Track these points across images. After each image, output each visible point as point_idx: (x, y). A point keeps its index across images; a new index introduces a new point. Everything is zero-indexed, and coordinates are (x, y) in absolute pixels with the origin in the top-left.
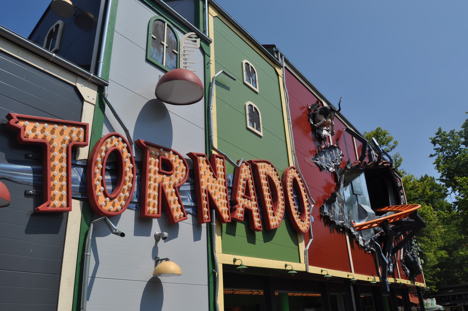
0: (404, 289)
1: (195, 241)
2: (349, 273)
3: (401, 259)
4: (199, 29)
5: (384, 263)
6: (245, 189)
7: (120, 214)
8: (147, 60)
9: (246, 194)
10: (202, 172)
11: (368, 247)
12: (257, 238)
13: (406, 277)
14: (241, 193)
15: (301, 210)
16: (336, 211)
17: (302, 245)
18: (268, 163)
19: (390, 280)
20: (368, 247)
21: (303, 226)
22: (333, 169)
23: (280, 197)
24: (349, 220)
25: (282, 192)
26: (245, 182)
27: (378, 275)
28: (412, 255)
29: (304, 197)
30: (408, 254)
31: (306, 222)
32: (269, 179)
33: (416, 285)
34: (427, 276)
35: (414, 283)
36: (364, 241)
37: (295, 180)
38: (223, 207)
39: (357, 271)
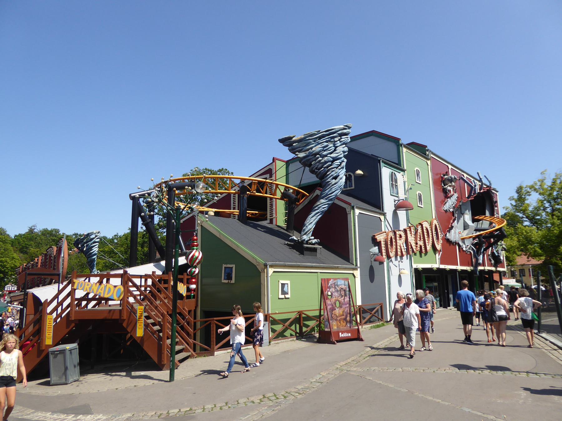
0: (490, 272)
1: (379, 265)
4: (401, 167)
8: (391, 195)
13: (491, 265)
14: (418, 239)
15: (438, 238)
17: (437, 255)
18: (427, 221)
19: (480, 268)
21: (439, 247)
23: (430, 236)
27: (472, 266)
28: (497, 251)
29: (439, 232)
30: (494, 251)
33: (498, 270)
34: (143, 214)
35: (497, 269)
36: (466, 248)
37: (436, 225)
39: (461, 265)
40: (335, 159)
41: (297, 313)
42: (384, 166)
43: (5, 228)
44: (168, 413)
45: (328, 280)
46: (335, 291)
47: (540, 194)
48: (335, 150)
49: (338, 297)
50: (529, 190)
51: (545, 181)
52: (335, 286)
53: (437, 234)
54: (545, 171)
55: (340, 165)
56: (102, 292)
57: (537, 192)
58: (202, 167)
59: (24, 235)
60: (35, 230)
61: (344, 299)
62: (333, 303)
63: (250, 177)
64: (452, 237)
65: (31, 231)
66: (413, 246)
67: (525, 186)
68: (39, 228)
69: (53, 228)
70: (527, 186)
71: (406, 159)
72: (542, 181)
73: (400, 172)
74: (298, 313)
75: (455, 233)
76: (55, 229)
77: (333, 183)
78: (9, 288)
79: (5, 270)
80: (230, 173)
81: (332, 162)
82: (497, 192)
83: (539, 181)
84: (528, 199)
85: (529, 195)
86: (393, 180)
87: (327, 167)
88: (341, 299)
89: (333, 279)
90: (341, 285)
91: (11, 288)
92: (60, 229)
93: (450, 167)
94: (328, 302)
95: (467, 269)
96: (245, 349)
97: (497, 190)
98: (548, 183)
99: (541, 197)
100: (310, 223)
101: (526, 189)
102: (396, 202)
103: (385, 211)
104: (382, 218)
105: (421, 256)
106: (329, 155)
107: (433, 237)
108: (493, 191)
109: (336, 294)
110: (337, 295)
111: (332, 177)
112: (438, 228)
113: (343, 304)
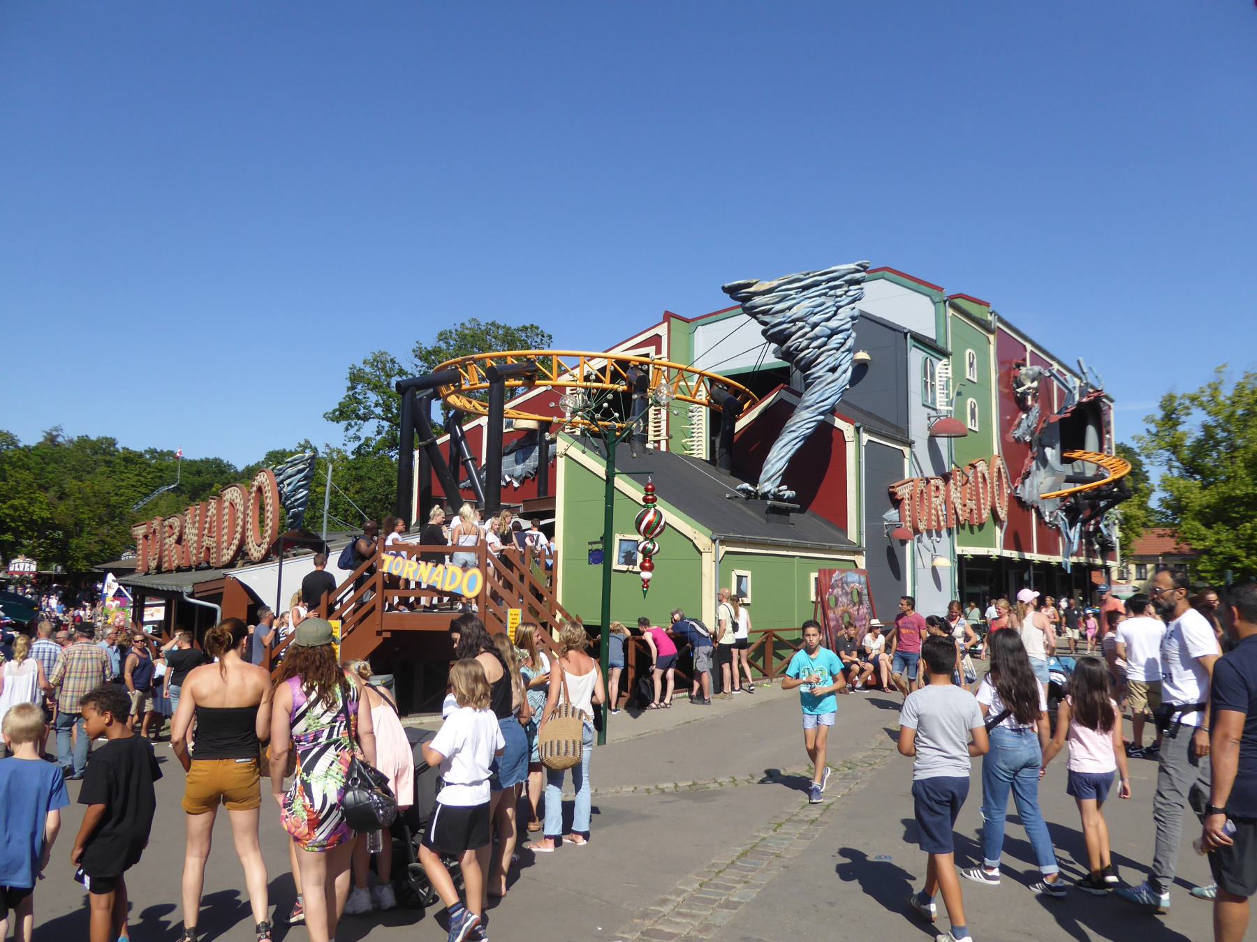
21: (1003, 514)
36: (1050, 516)
40: (835, 332)
41: (762, 633)
42: (914, 346)
43: (14, 434)
44: (676, 786)
45: (831, 572)
46: (843, 593)
47: (1209, 413)
48: (835, 314)
49: (848, 605)
50: (1187, 403)
51: (1221, 387)
52: (842, 583)
53: (1000, 486)
54: (1224, 366)
55: (843, 344)
56: (439, 580)
57: (1204, 409)
58: (484, 321)
59: (36, 448)
60: (60, 439)
61: (858, 610)
62: (838, 617)
63: (606, 351)
64: (1027, 493)
65: (51, 439)
66: (958, 510)
67: (1179, 395)
68: (71, 432)
69: (103, 435)
70: (1184, 396)
71: (952, 332)
72: (1216, 389)
73: (941, 357)
74: (766, 633)
75: (1032, 486)
76: (106, 439)
77: (829, 381)
78: (19, 567)
79: (18, 526)
80: (545, 335)
81: (830, 337)
82: (1112, 401)
83: (1209, 386)
84: (1184, 422)
85: (1188, 414)
86: (928, 373)
87: (819, 347)
88: (853, 610)
89: (839, 570)
90: (853, 582)
91: (22, 566)
92: (118, 439)
93: (1029, 347)
94: (831, 615)
95: (1012, 556)
96: (682, 697)
97: (1112, 396)
98: (1227, 392)
99: (1210, 420)
100: (779, 457)
101: (1182, 401)
102: (932, 419)
103: (913, 437)
104: (906, 450)
105: (972, 532)
106: (823, 324)
107: (993, 493)
108: (1104, 400)
109: (844, 600)
110: (845, 601)
111: (827, 368)
112: (1003, 475)
113: (855, 620)
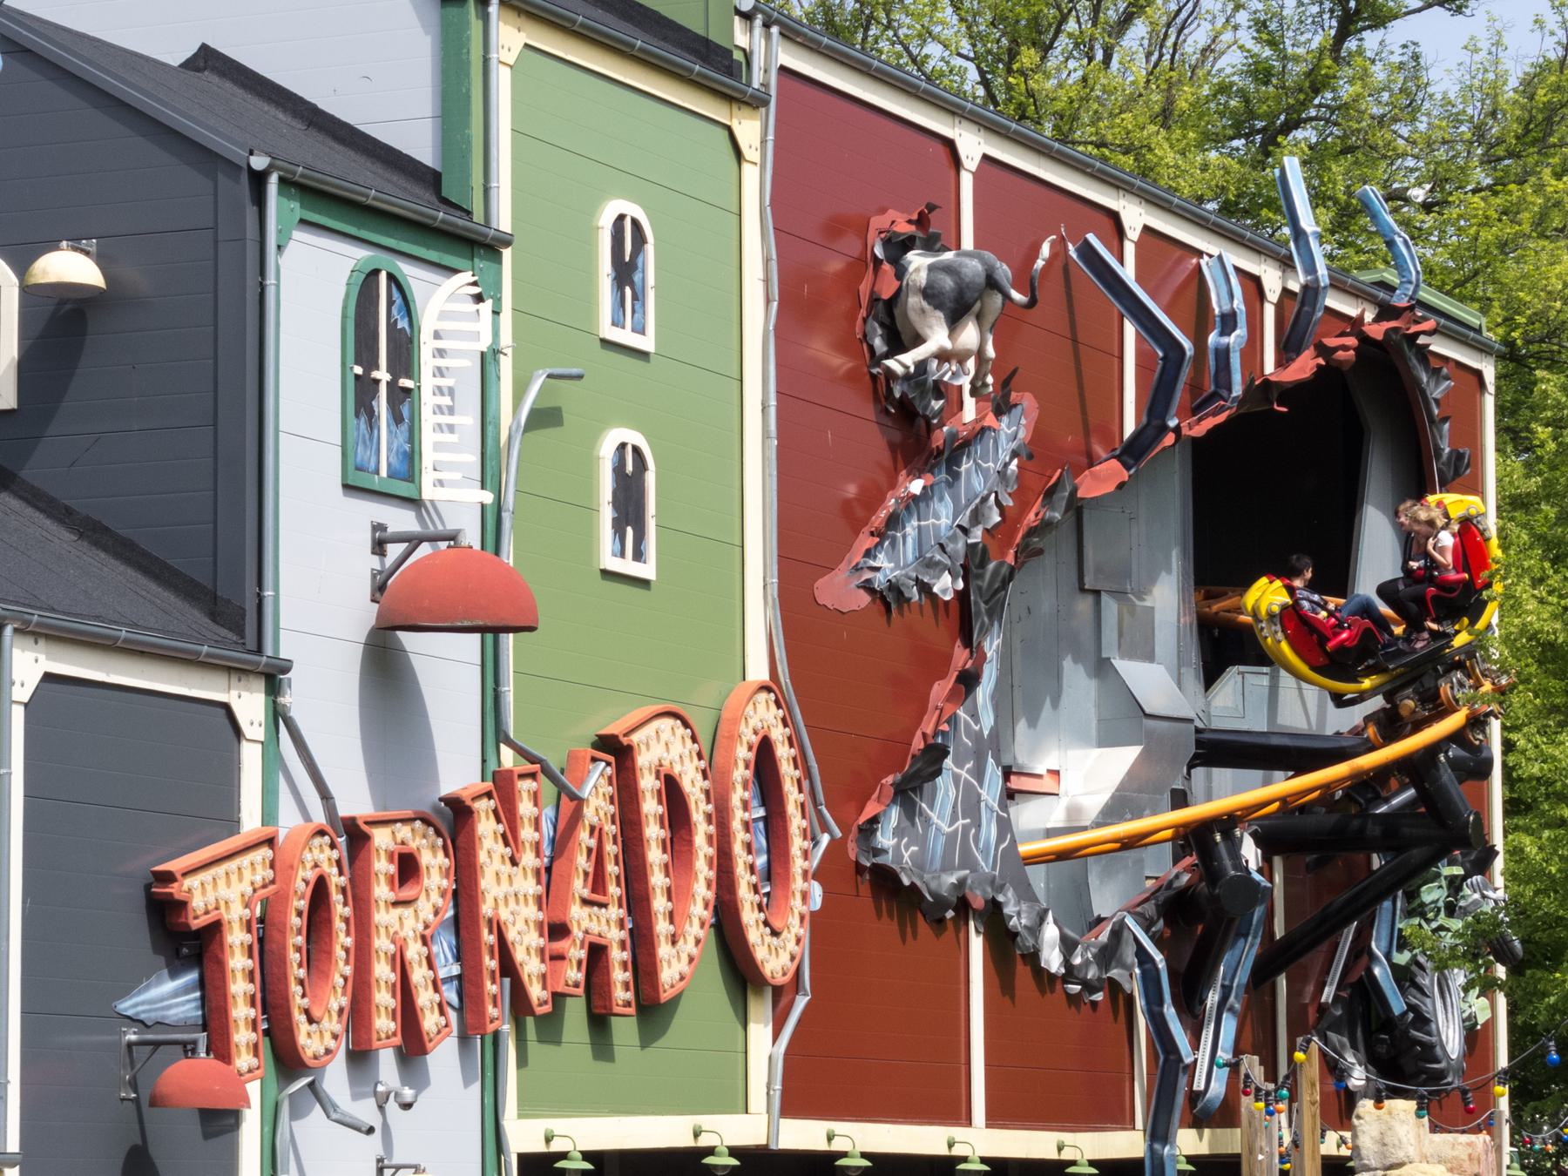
2: (957, 1132)
3: (1195, 1088)
5: (1172, 1057)
6: (591, 870)
7: (324, 1066)
9: (594, 890)
10: (482, 857)
11: (1089, 976)
12: (616, 1040)
15: (775, 872)
16: (935, 819)
17: (760, 1033)
18: (686, 725)
20: (1089, 976)
22: (954, 579)
23: (703, 849)
24: (1000, 839)
25: (712, 829)
26: (593, 843)
31: (789, 939)
32: (672, 791)
37: (765, 751)
38: (531, 966)
